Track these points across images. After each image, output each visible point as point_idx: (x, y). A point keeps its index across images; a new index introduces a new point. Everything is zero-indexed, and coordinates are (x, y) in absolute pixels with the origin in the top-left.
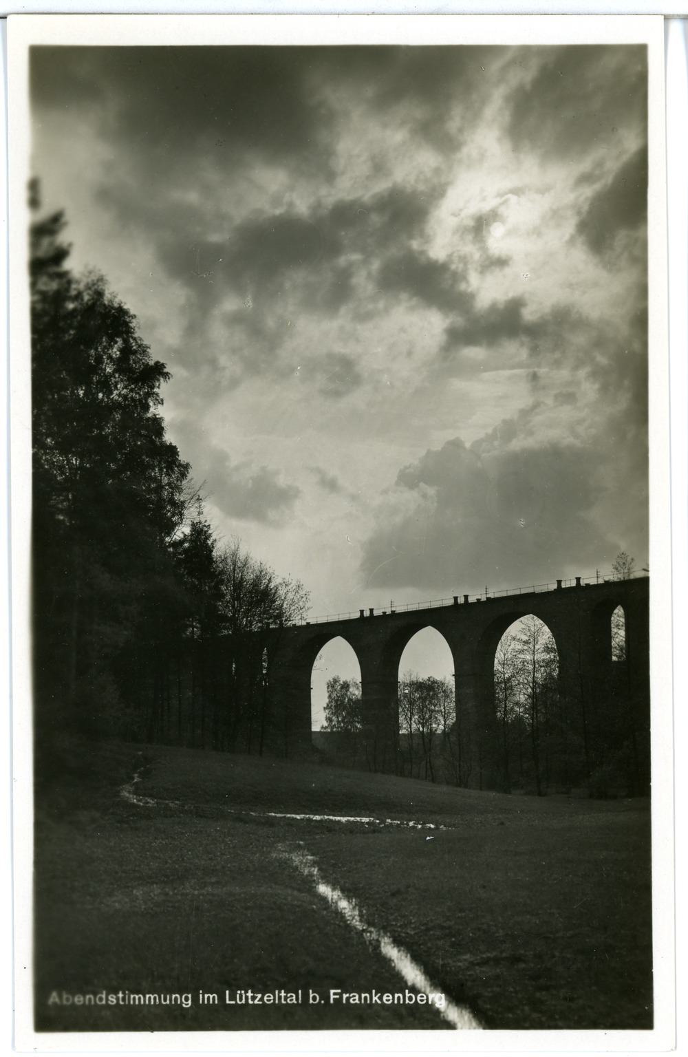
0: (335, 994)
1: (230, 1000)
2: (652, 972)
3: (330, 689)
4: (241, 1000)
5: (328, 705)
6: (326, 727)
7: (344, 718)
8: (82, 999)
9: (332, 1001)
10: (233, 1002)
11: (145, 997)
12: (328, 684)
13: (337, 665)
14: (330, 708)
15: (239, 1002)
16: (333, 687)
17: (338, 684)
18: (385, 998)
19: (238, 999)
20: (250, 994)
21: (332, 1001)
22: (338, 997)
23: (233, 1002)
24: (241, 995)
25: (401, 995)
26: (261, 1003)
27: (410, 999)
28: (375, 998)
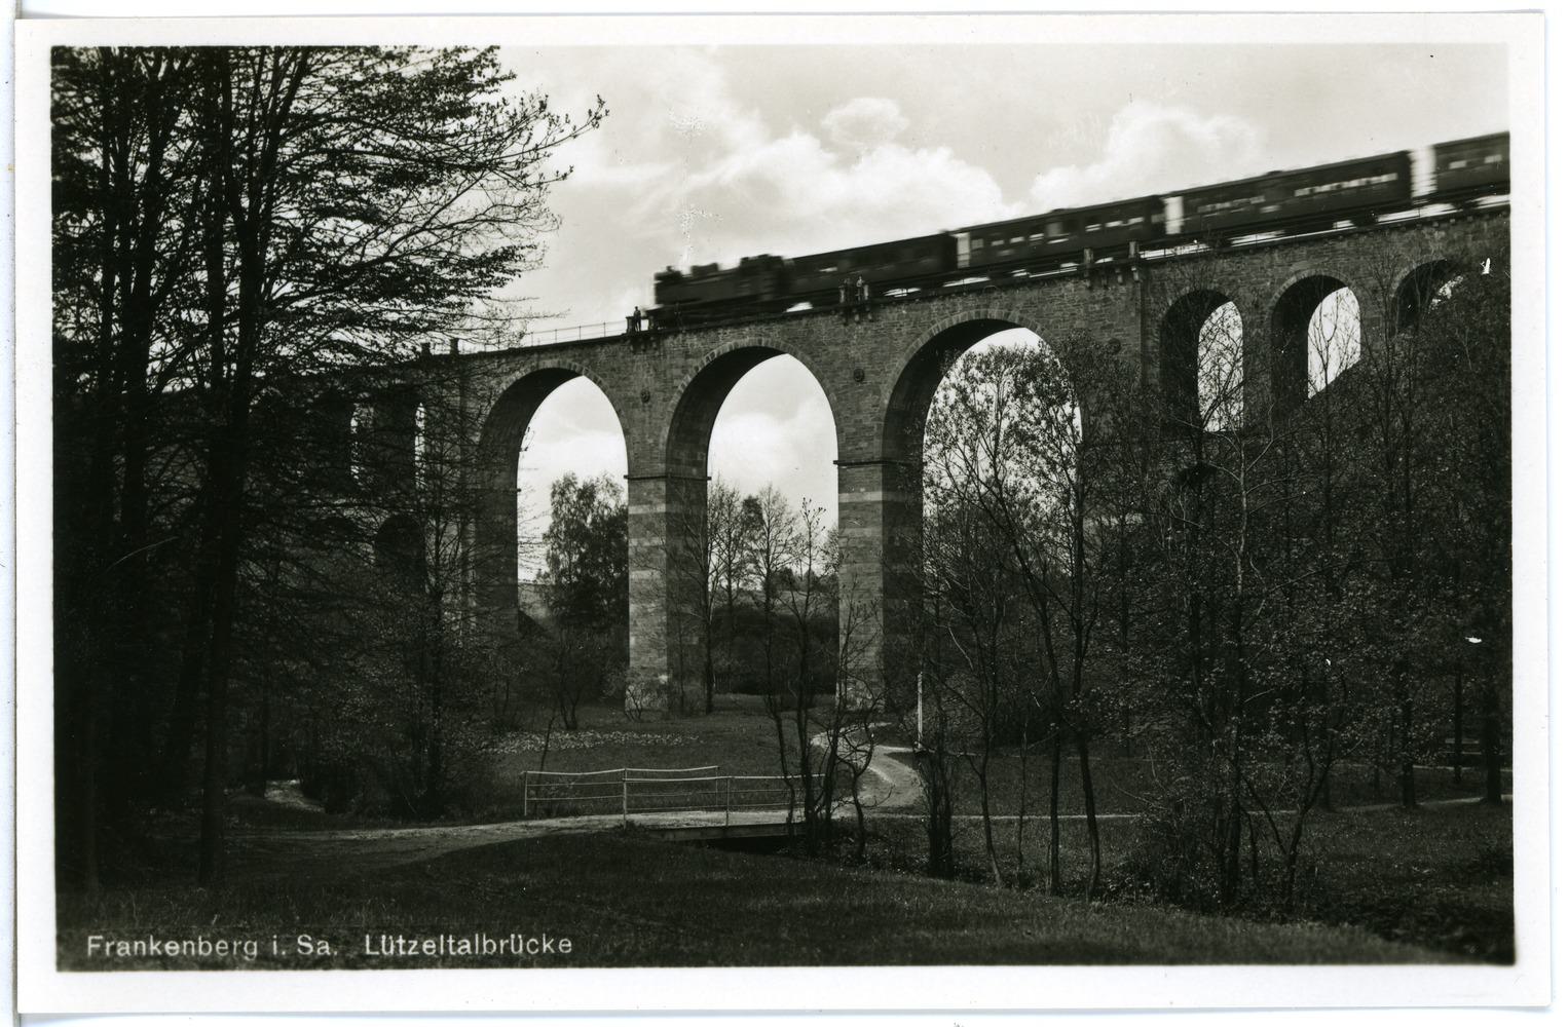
0: (94, 941)
1: (372, 949)
2: (54, 363)
3: (557, 498)
4: (388, 949)
5: (552, 531)
6: (547, 575)
7: (583, 557)
8: (177, 947)
9: (90, 953)
10: (377, 953)
11: (132, 945)
12: (554, 486)
13: (575, 445)
14: (556, 536)
15: (385, 953)
16: (563, 494)
17: (572, 489)
18: (425, 946)
19: (383, 950)
20: (401, 941)
21: (90, 953)
22: (98, 946)
23: (377, 953)
24: (388, 942)
25: (143, 943)
26: (416, 953)
27: (490, 946)
28: (546, 946)
